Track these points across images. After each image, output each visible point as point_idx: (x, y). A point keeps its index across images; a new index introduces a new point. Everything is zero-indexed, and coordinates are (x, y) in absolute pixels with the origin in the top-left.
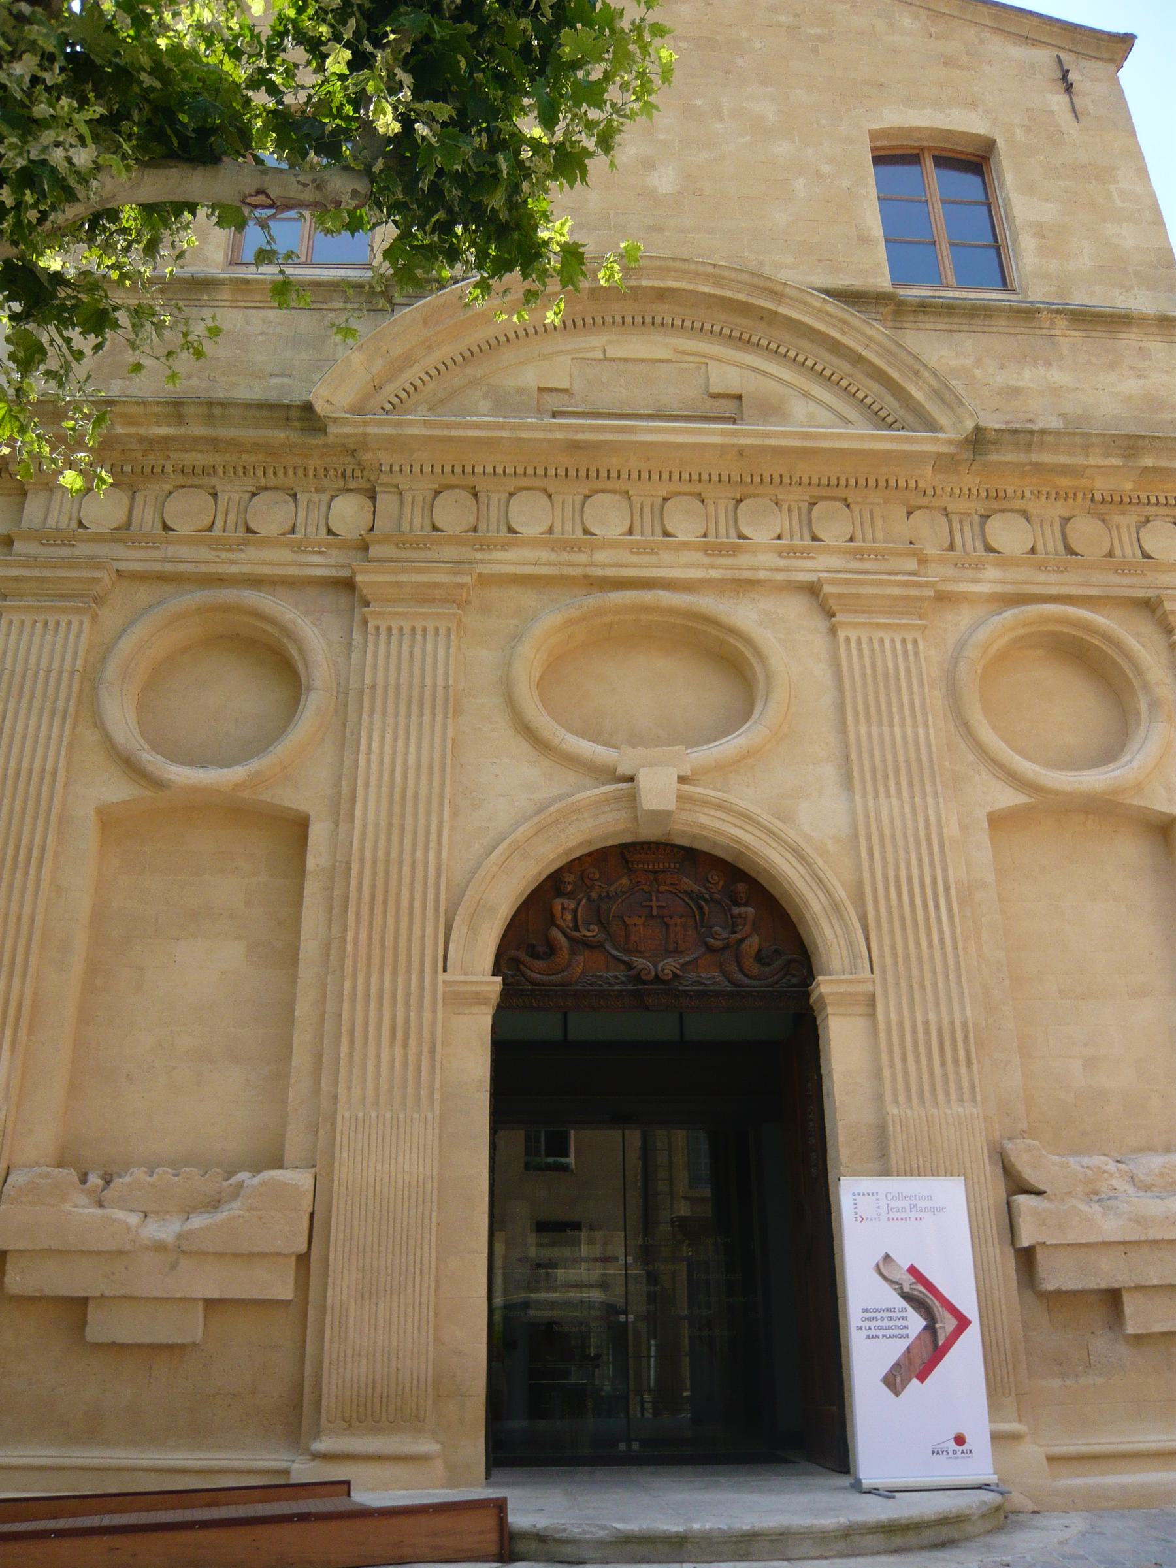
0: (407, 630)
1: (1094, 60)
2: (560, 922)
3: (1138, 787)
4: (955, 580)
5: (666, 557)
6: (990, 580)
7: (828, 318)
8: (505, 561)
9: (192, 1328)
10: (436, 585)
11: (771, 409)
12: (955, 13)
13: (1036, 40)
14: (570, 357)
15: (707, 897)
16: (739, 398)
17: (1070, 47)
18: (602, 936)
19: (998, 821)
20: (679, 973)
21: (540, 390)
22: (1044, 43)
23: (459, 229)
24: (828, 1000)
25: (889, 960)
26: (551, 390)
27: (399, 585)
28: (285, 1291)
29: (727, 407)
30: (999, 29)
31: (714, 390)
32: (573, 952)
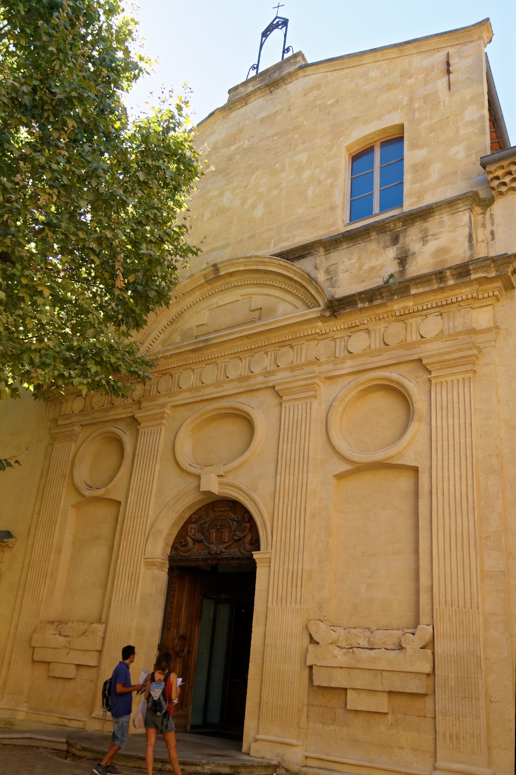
0: (150, 432)
1: (469, 44)
2: (190, 534)
3: (400, 454)
4: (333, 371)
5: (226, 386)
6: (349, 365)
7: (282, 267)
8: (180, 399)
9: (71, 672)
10: (156, 414)
11: (272, 311)
12: (398, 55)
13: (439, 48)
14: (206, 310)
15: (236, 520)
16: (261, 308)
17: (457, 42)
18: (203, 538)
19: (339, 477)
20: (224, 551)
21: (197, 326)
22: (443, 48)
23: (78, 334)
24: (257, 561)
25: (278, 544)
26: (201, 325)
27: (146, 416)
28: (93, 663)
29: (256, 314)
30: (420, 52)
31: (252, 309)
32: (194, 544)
